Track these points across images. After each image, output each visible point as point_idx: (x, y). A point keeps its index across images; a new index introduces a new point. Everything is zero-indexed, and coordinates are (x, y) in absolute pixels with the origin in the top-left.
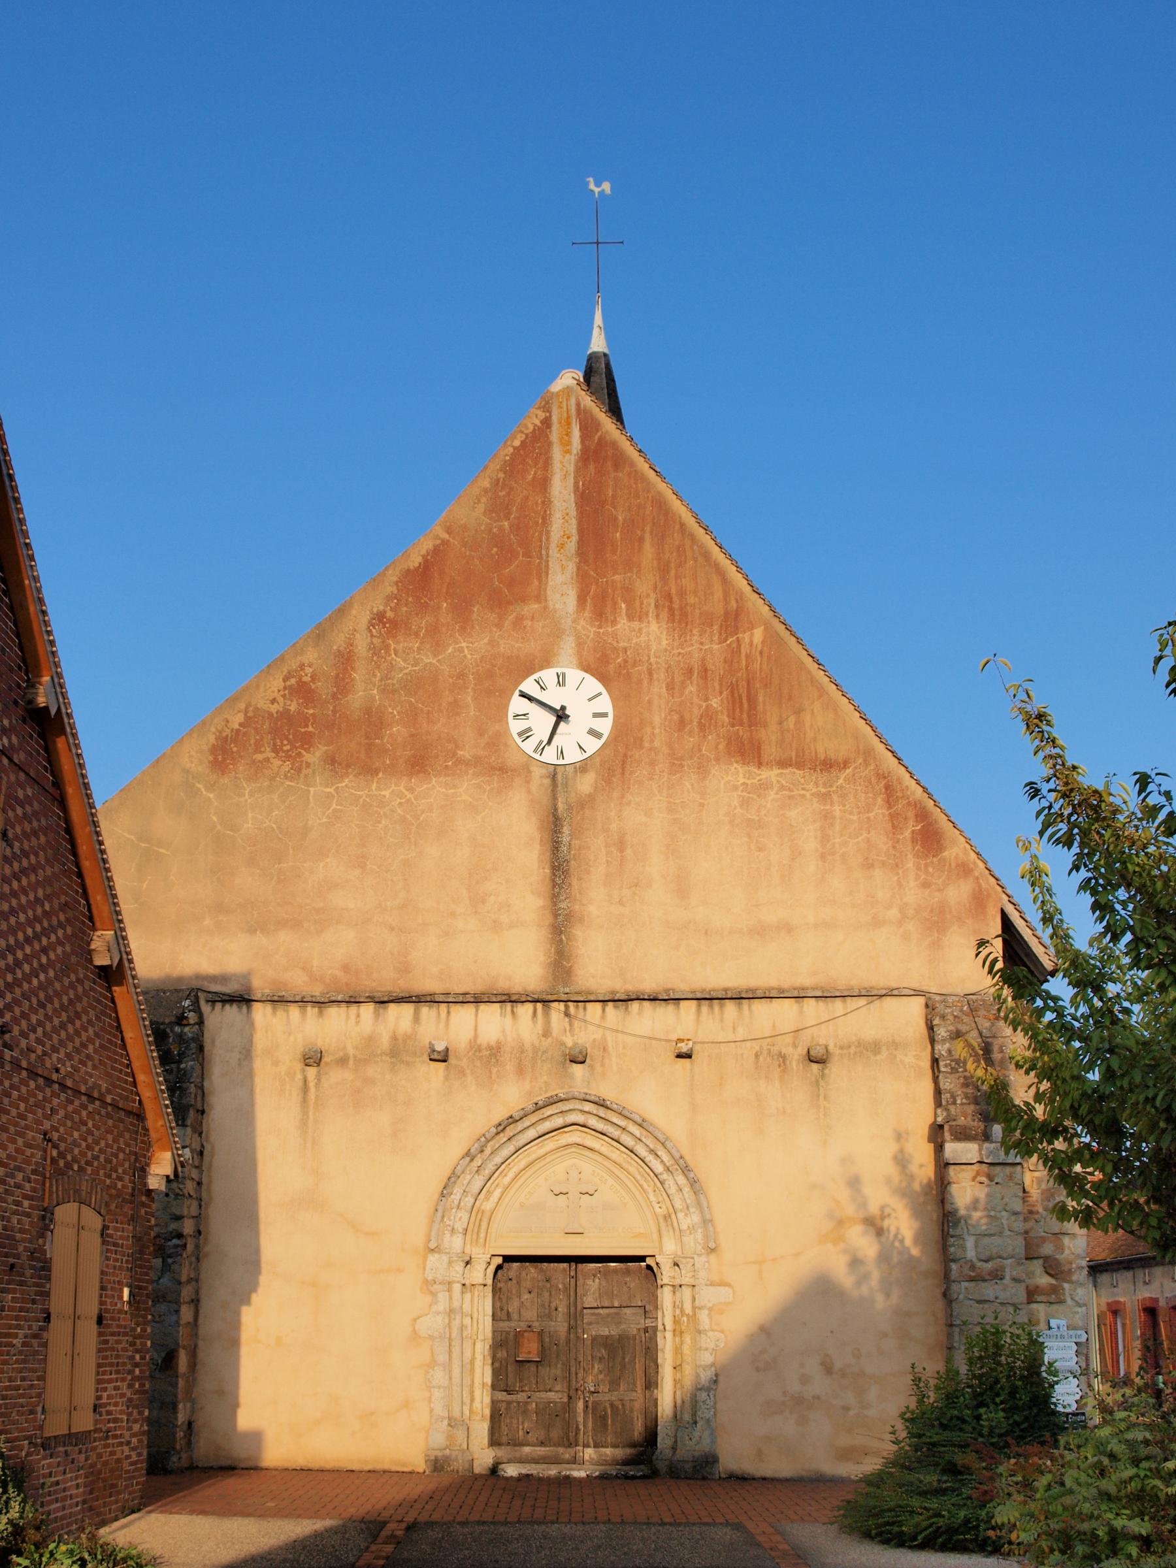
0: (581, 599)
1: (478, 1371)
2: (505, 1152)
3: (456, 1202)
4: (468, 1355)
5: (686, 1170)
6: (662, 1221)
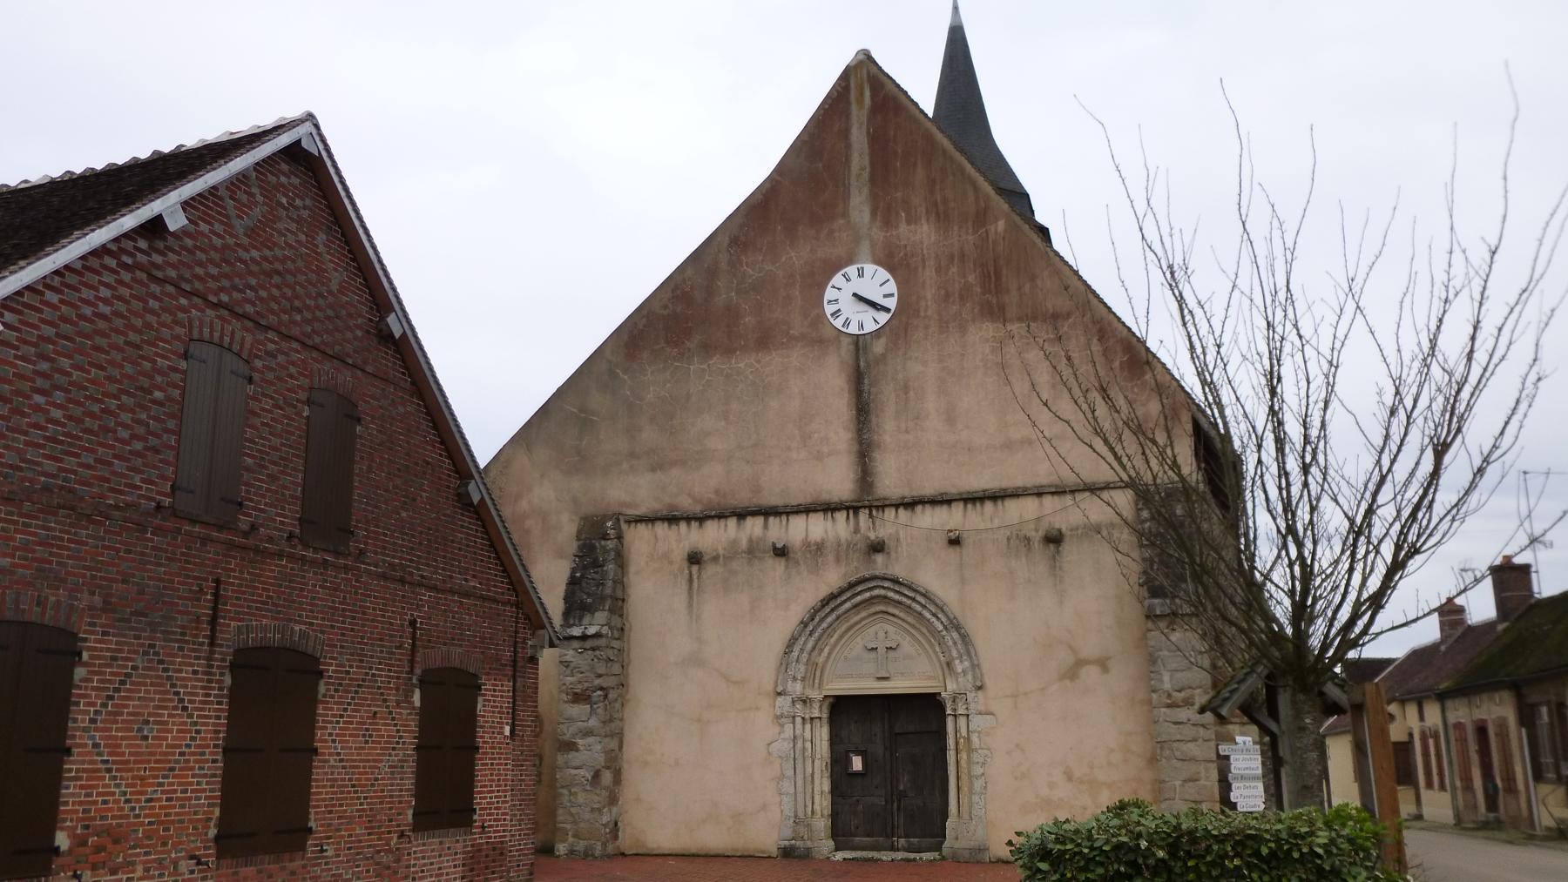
0: (874, 213)
1: (817, 782)
2: (829, 620)
5: (958, 628)
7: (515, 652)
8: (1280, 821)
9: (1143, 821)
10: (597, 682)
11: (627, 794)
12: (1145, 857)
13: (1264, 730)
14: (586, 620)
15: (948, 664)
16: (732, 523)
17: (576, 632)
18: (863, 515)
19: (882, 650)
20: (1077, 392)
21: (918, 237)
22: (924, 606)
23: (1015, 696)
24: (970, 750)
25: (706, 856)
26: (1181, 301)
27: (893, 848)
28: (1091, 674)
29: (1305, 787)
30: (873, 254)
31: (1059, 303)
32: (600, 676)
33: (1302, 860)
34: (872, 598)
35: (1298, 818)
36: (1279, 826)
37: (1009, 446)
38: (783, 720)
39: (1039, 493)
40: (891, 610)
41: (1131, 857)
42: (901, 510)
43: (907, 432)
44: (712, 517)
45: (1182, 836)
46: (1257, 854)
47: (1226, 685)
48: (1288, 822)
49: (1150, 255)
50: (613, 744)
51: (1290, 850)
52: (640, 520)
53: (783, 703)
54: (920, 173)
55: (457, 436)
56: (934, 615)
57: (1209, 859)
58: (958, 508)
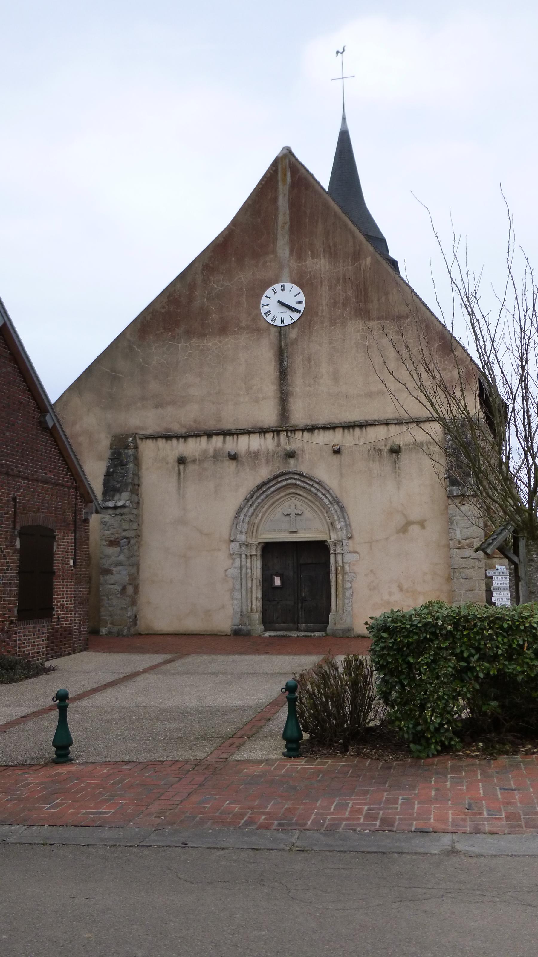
0: (291, 251)
1: (254, 592)
2: (262, 497)
3: (242, 520)
4: (249, 585)
5: (338, 503)
6: (330, 525)
7: (75, 516)
8: (515, 610)
9: (440, 610)
10: (124, 534)
11: (142, 599)
12: (441, 630)
13: (511, 561)
14: (116, 498)
15: (332, 524)
16: (204, 439)
17: (111, 504)
18: (283, 435)
19: (293, 516)
20: (411, 367)
21: (318, 266)
22: (318, 490)
23: (370, 542)
24: (344, 574)
25: (189, 635)
26: (471, 314)
27: (298, 630)
28: (415, 529)
29: (531, 592)
30: (291, 276)
31: (404, 310)
32: (125, 530)
33: (525, 630)
34: (288, 485)
35: (525, 608)
36: (514, 613)
37: (370, 395)
38: (234, 556)
39: (387, 424)
40: (299, 492)
41: (433, 630)
42: (305, 433)
43: (309, 386)
44: (192, 436)
45: (461, 618)
46: (501, 627)
47: (490, 536)
48: (519, 611)
49: (454, 286)
50: (133, 570)
51: (519, 625)
52: (154, 437)
53: (234, 546)
54: (320, 227)
55: (38, 386)
56: (324, 495)
57: (475, 630)
58: (339, 432)
